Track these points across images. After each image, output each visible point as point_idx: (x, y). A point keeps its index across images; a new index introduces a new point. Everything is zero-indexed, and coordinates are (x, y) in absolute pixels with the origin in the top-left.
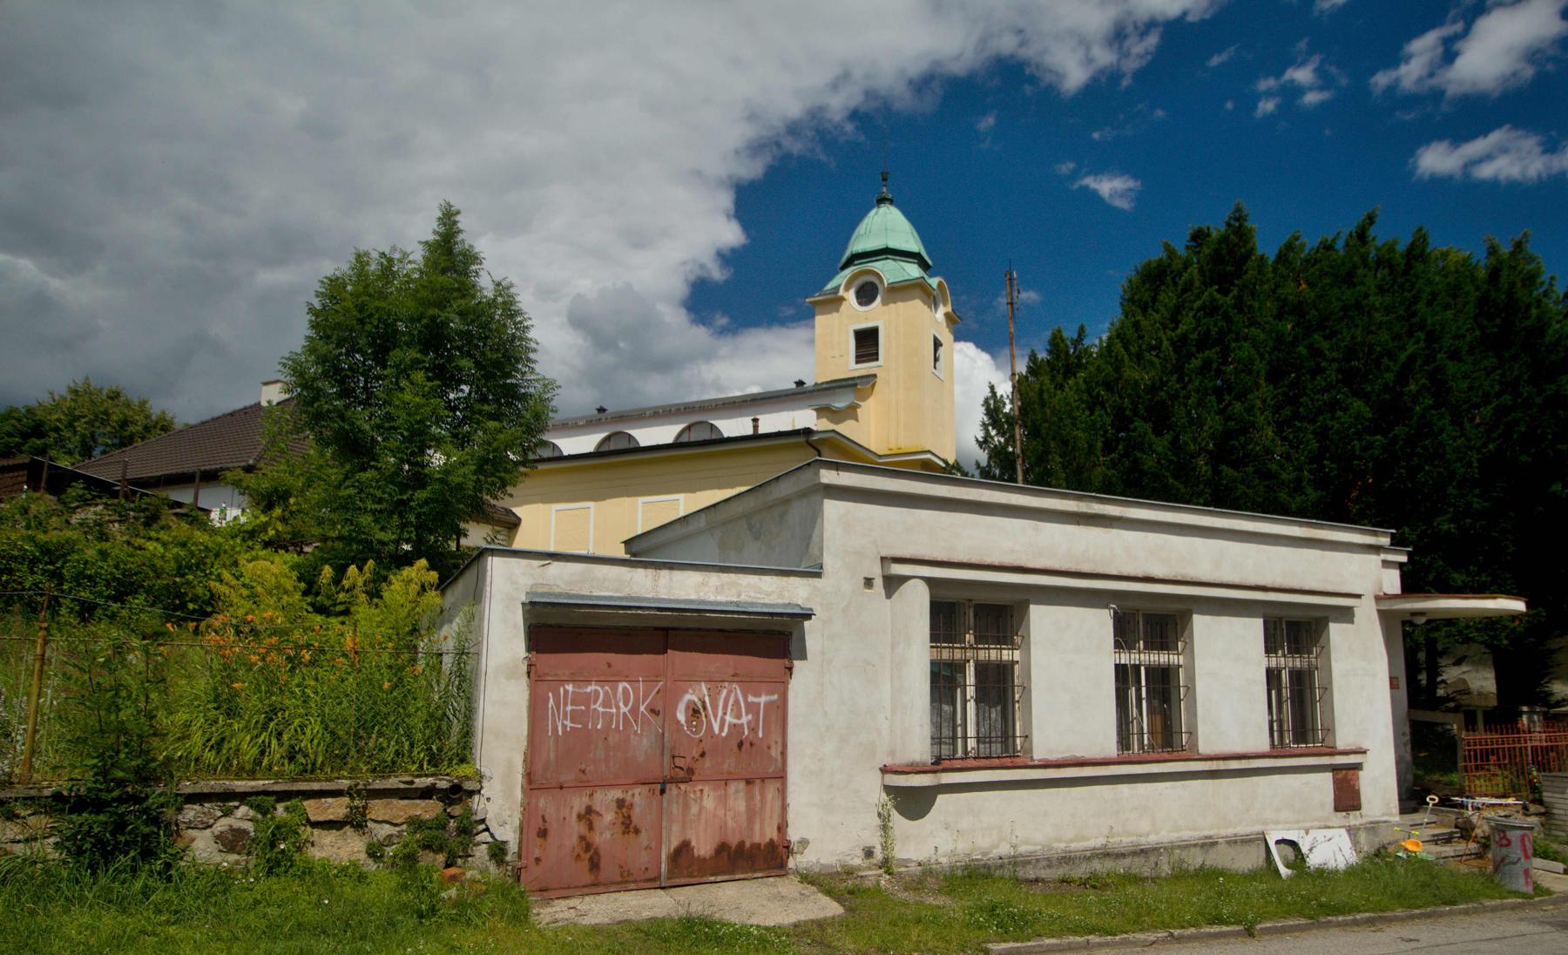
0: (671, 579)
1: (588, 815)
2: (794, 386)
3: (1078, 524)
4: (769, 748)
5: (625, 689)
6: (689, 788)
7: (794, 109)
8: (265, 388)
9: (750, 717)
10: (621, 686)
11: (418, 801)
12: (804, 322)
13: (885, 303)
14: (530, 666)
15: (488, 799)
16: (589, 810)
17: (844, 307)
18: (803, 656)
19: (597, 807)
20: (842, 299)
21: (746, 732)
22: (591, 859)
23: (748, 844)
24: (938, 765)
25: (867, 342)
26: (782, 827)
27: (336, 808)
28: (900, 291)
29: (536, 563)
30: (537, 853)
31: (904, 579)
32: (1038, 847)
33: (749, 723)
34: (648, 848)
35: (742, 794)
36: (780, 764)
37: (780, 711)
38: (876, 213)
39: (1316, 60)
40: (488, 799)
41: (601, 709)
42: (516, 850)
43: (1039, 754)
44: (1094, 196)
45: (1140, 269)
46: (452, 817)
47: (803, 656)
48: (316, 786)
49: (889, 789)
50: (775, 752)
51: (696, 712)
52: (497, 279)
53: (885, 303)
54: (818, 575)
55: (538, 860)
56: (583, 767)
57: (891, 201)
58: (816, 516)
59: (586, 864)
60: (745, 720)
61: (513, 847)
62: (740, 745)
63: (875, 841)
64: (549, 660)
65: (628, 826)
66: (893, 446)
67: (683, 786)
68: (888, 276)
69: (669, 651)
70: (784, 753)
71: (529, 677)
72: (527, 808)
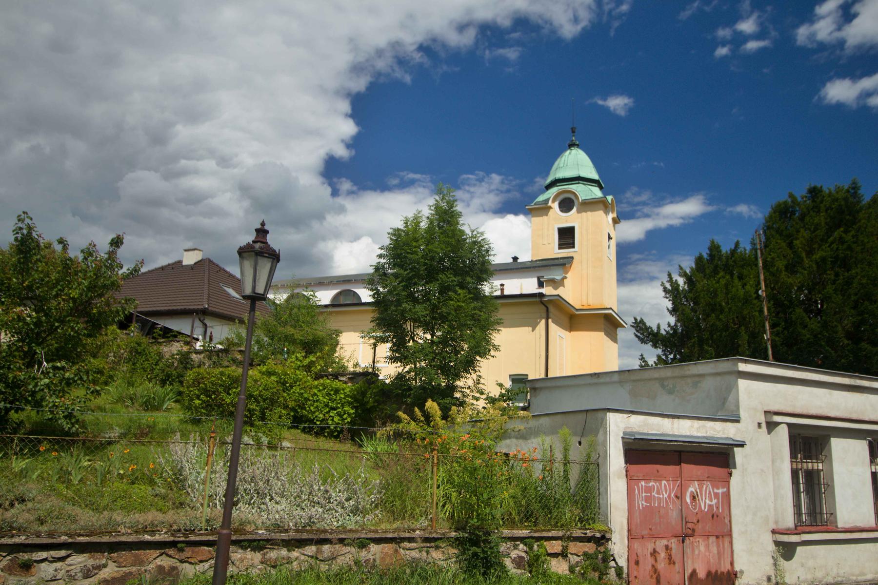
0: (679, 424)
1: (654, 553)
2: (511, 260)
3: (849, 391)
4: (724, 518)
5: (665, 484)
6: (694, 540)
7: (382, 41)
8: (185, 253)
9: (716, 500)
10: (664, 482)
11: (586, 544)
12: (407, 189)
13: (579, 212)
14: (626, 471)
15: (614, 543)
16: (655, 551)
17: (551, 212)
18: (735, 467)
19: (657, 550)
20: (550, 208)
21: (715, 509)
22: (657, 578)
23: (719, 572)
24: (796, 531)
25: (567, 236)
26: (732, 564)
27: (556, 547)
28: (589, 205)
29: (626, 416)
30: (635, 573)
31: (778, 424)
32: (844, 579)
33: (716, 504)
34: (679, 572)
35: (715, 544)
36: (729, 527)
37: (727, 496)
38: (570, 154)
39: (754, 16)
40: (614, 543)
41: (656, 496)
42: (627, 572)
43: (840, 524)
44: (606, 110)
45: (774, 206)
46: (601, 552)
47: (735, 467)
48: (550, 534)
49: (777, 543)
50: (727, 521)
51: (694, 497)
52: (473, 228)
53: (579, 212)
54: (738, 421)
55: (636, 577)
56: (650, 527)
57: (578, 146)
58: (732, 388)
59: (654, 580)
60: (714, 502)
61: (625, 570)
62: (713, 516)
63: (772, 573)
64: (634, 468)
65: (671, 561)
66: (585, 303)
67: (691, 538)
68: (582, 195)
69: (682, 464)
70: (730, 521)
71: (627, 477)
72: (629, 548)
